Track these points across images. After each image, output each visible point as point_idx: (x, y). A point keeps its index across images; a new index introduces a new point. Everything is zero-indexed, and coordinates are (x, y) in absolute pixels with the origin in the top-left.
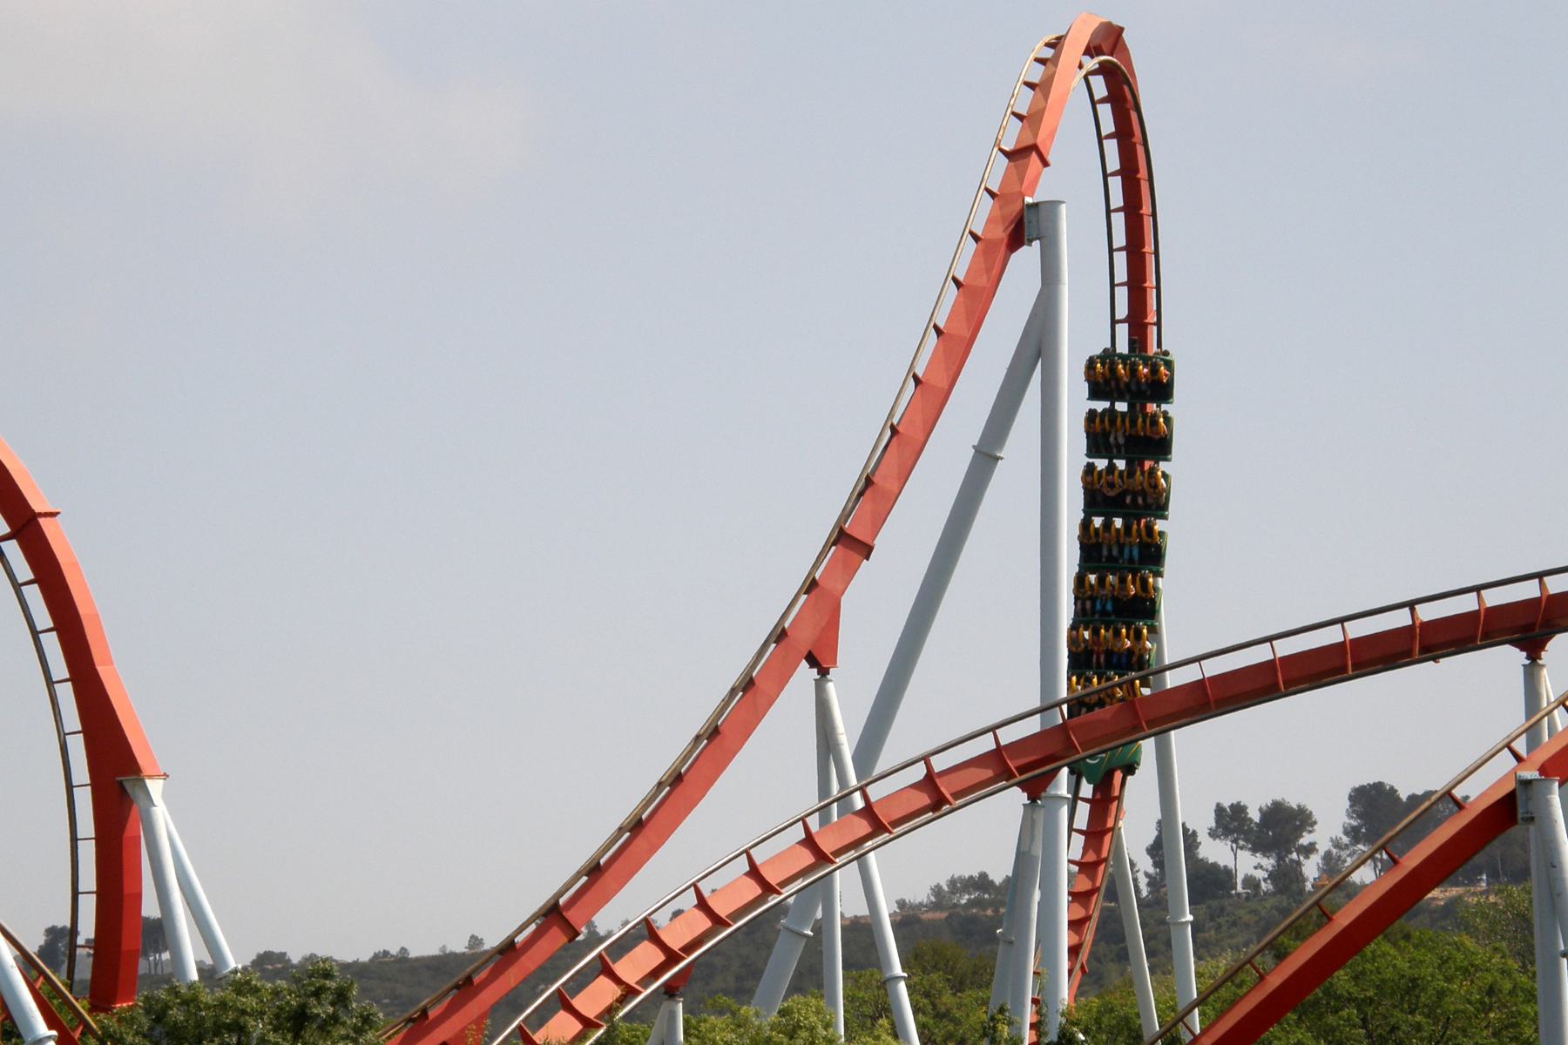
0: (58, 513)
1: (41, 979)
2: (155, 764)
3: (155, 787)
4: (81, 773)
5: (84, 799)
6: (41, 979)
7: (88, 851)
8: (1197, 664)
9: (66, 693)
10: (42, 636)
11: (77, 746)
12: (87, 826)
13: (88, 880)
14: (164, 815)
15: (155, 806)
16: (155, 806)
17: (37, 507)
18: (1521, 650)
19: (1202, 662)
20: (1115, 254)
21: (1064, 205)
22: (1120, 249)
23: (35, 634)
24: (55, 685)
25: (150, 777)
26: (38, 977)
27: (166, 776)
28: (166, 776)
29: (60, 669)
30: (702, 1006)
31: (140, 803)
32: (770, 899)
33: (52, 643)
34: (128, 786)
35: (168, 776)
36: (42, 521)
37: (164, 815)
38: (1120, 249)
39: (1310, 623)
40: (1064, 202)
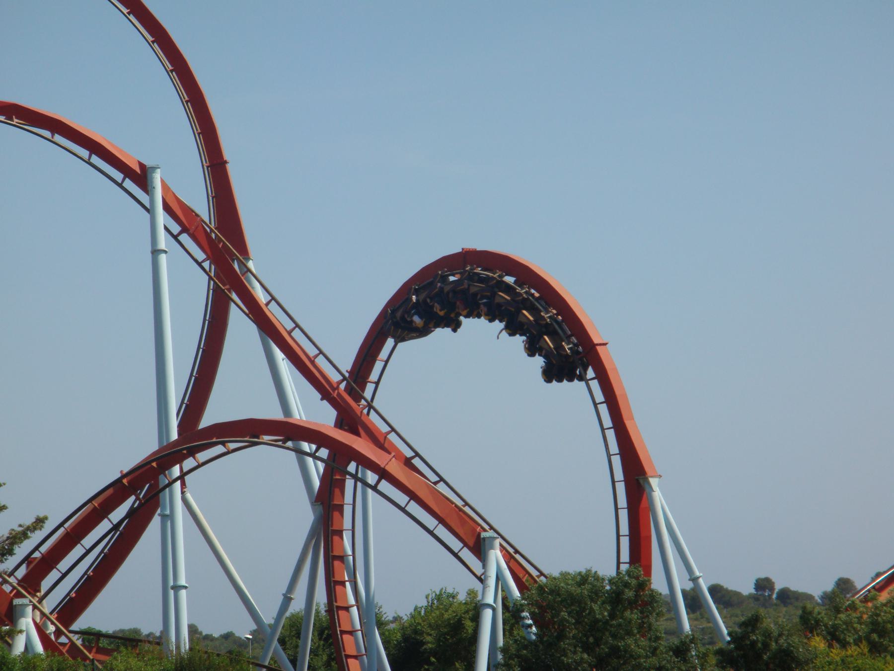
0: (606, 344)
1: (527, 575)
2: (654, 469)
3: (654, 482)
4: (619, 475)
5: (621, 488)
6: (527, 575)
7: (624, 515)
8: (621, 537)
9: (611, 435)
10: (599, 406)
11: (617, 461)
12: (623, 501)
13: (625, 529)
14: (661, 501)
15: (654, 491)
16: (654, 491)
17: (596, 341)
18: (491, 320)
19: (351, 531)
20: (124, 185)
21: (158, 170)
22: (123, 180)
23: (595, 405)
24: (606, 431)
25: (652, 477)
26: (525, 575)
27: (660, 476)
28: (660, 476)
29: (607, 422)
30: (22, 662)
31: (647, 490)
32: (171, 649)
33: (604, 409)
34: (641, 481)
35: (661, 476)
36: (598, 348)
37: (661, 501)
38: (123, 180)
39: (209, 464)
40: (159, 168)
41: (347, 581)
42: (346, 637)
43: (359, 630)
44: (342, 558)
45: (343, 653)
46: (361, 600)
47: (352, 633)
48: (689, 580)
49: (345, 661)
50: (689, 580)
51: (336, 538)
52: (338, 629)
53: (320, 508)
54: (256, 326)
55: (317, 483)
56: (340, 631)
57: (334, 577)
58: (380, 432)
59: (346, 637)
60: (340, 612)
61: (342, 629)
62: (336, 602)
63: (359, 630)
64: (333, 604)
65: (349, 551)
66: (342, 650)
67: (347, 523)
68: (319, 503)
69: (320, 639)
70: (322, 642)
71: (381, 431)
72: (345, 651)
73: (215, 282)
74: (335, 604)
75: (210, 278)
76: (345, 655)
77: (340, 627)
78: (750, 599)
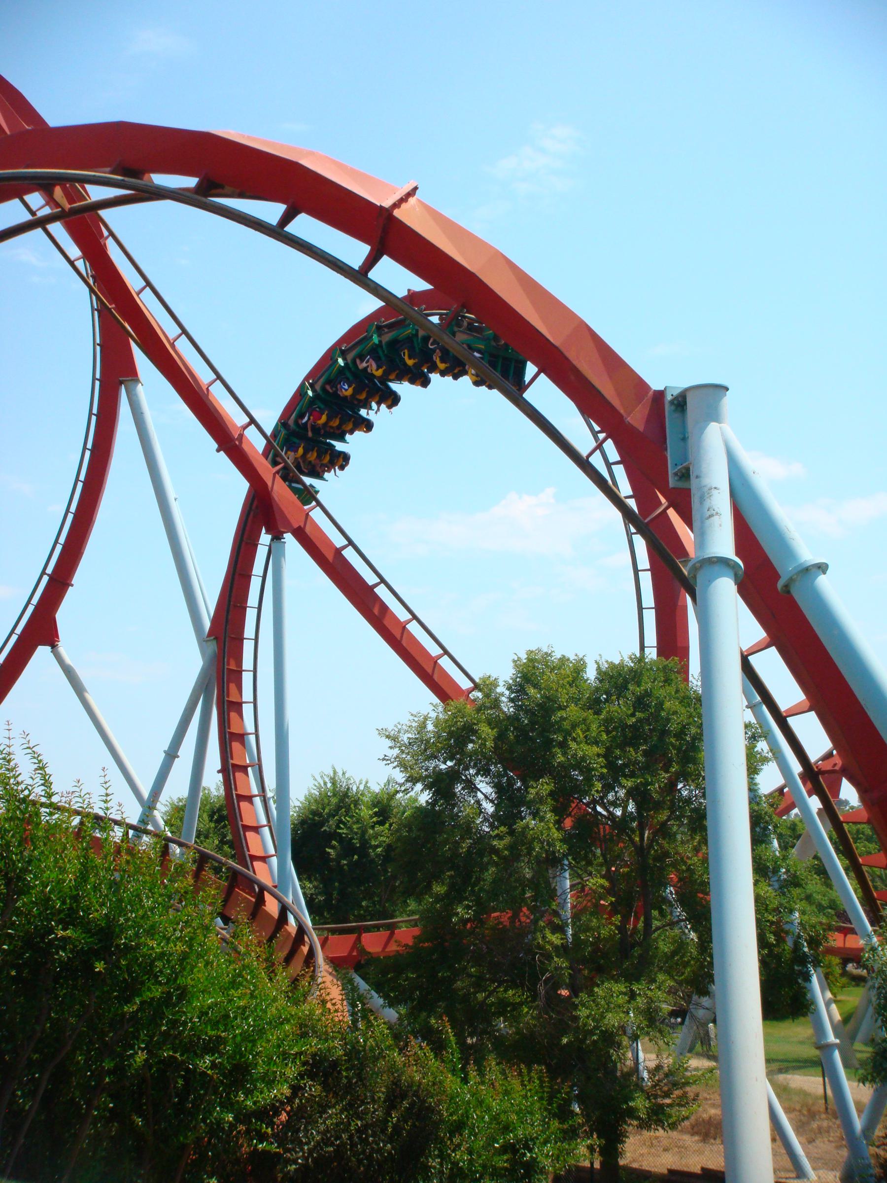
0: (416, 188)
41: (256, 796)
42: (250, 835)
43: (264, 826)
44: (241, 737)
45: (240, 823)
46: (273, 818)
47: (264, 859)
48: (747, 707)
49: (242, 833)
50: (747, 707)
51: (233, 715)
52: (234, 792)
53: (213, 647)
54: (109, 253)
55: (207, 624)
56: (237, 795)
57: (229, 728)
58: (235, 425)
59: (250, 835)
60: (255, 863)
61: (239, 792)
62: (232, 759)
63: (264, 826)
64: (227, 761)
65: (249, 727)
66: (245, 849)
67: (247, 694)
68: (212, 638)
69: (211, 821)
70: (213, 825)
71: (236, 425)
72: (242, 820)
73: (98, 298)
74: (231, 761)
75: (92, 291)
76: (237, 795)
77: (236, 790)
78: (874, 1178)
